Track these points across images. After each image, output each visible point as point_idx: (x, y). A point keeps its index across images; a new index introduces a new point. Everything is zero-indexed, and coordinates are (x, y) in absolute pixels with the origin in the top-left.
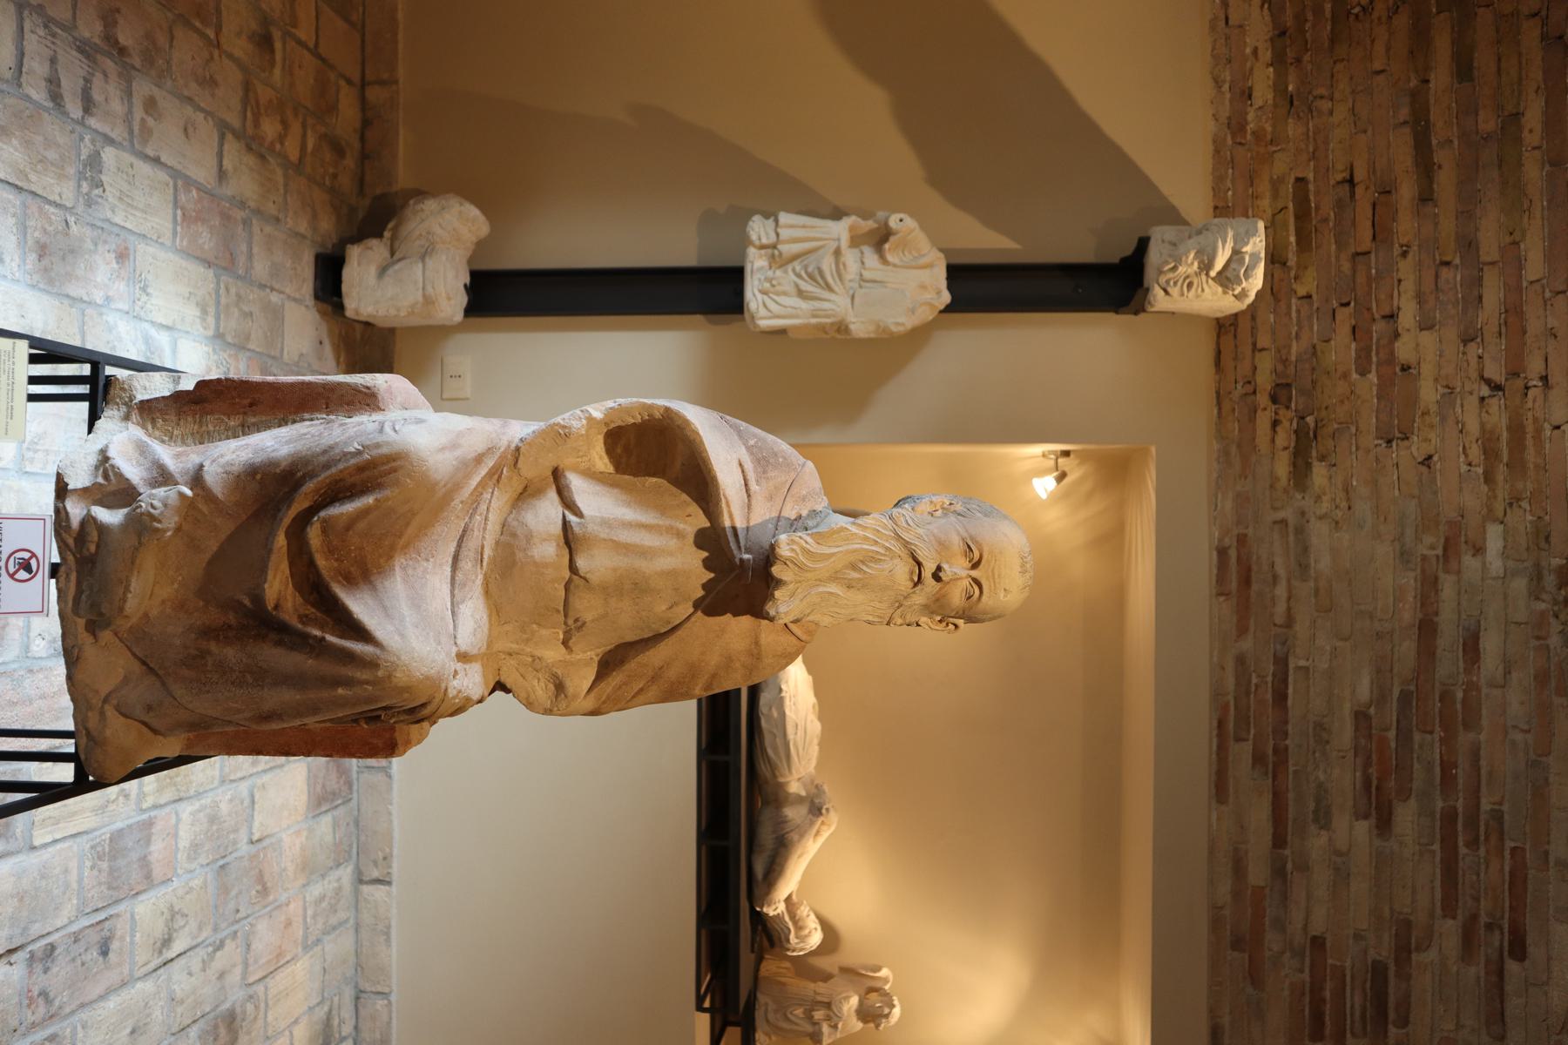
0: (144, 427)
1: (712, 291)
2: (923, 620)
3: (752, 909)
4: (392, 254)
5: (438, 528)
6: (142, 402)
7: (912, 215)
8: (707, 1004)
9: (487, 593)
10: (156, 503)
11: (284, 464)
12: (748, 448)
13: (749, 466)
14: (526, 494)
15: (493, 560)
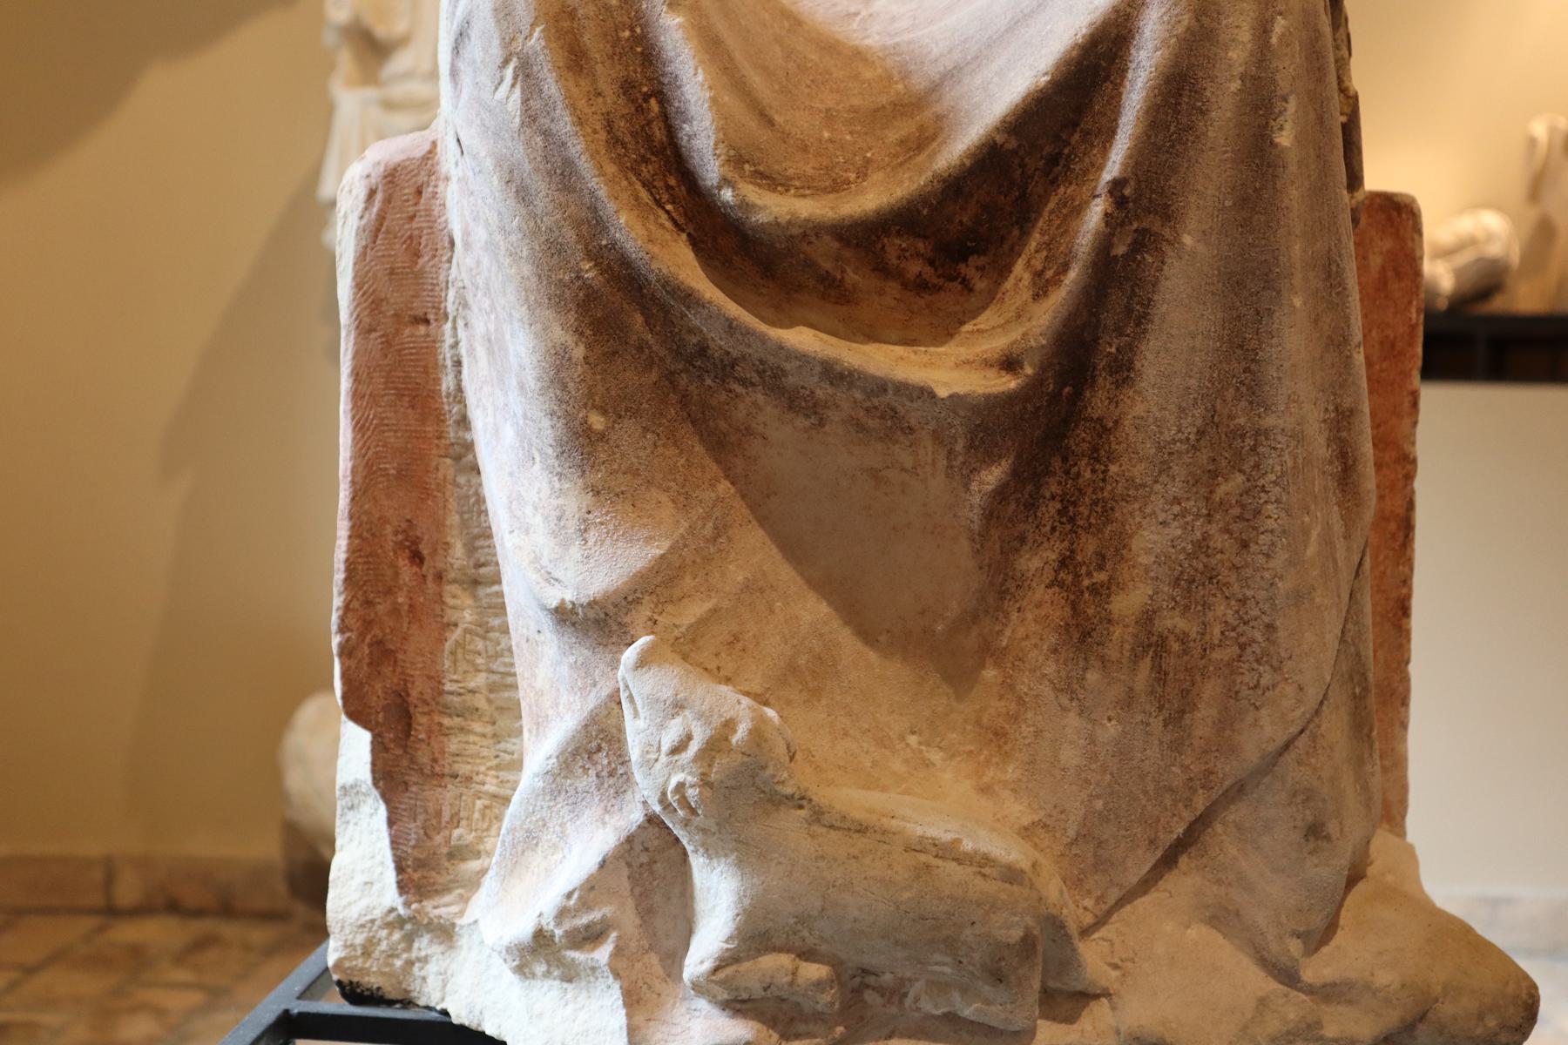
0: (474, 883)
6: (402, 887)
10: (669, 739)
11: (560, 335)
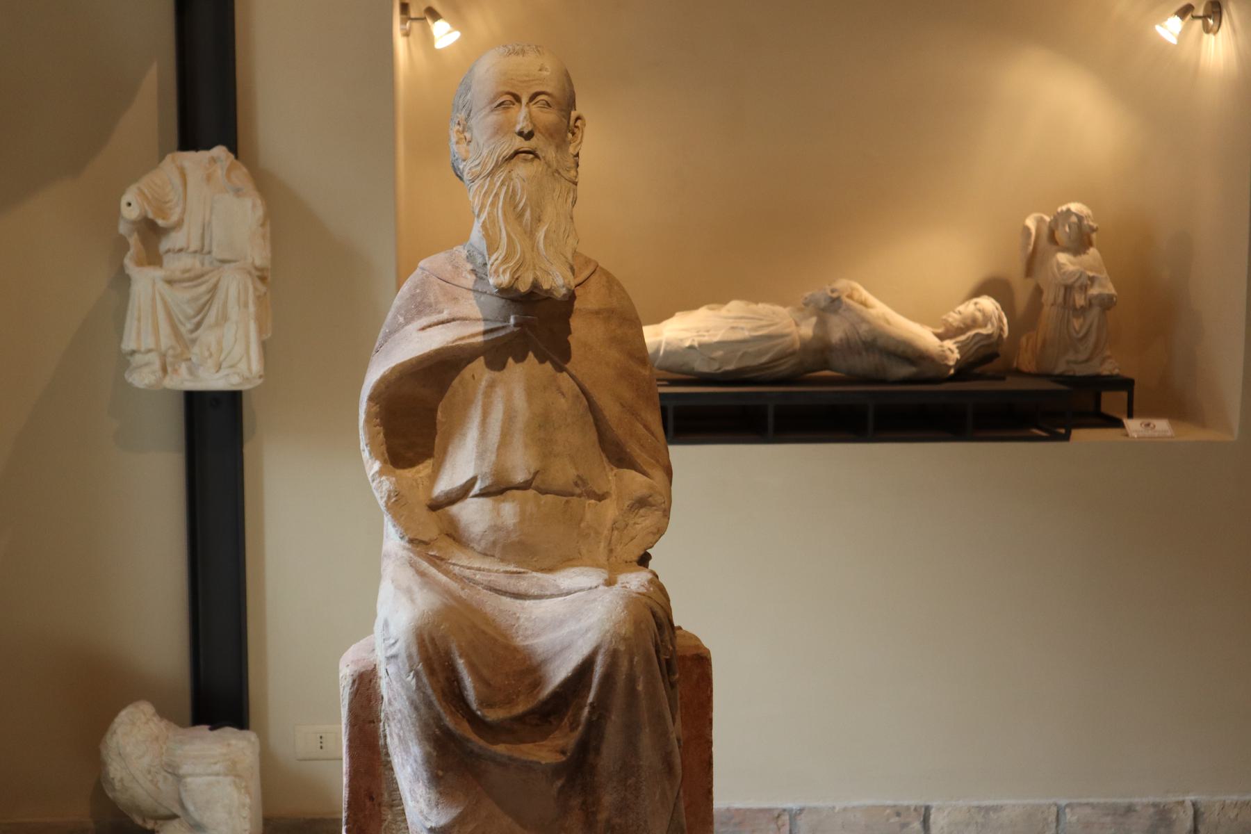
1: (213, 430)
2: (572, 150)
4: (174, 817)
5: (488, 609)
7: (122, 193)
8: (1063, 431)
9: (550, 570)
11: (428, 748)
12: (408, 321)
13: (424, 321)
14: (455, 534)
15: (518, 564)
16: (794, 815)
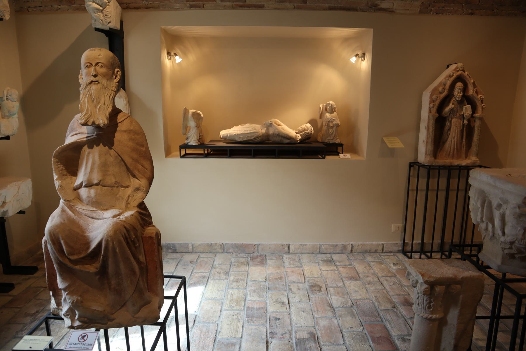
3: (299, 143)
13: (72, 134)
14: (79, 198)
15: (97, 208)
16: (258, 245)
